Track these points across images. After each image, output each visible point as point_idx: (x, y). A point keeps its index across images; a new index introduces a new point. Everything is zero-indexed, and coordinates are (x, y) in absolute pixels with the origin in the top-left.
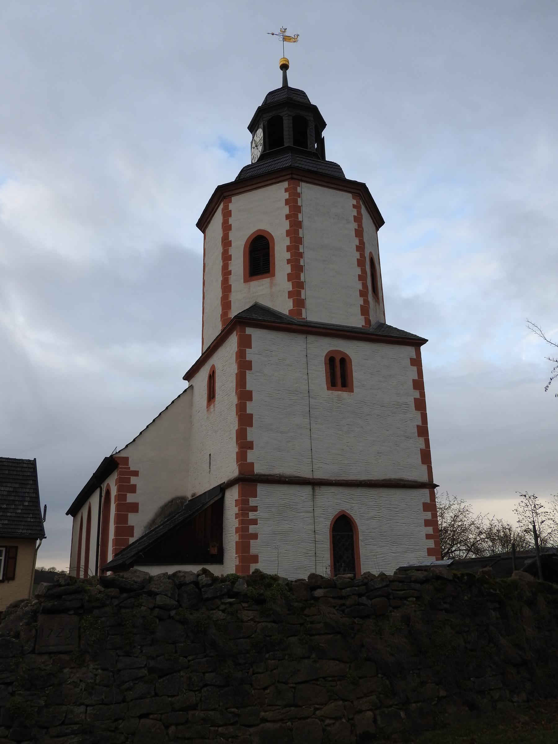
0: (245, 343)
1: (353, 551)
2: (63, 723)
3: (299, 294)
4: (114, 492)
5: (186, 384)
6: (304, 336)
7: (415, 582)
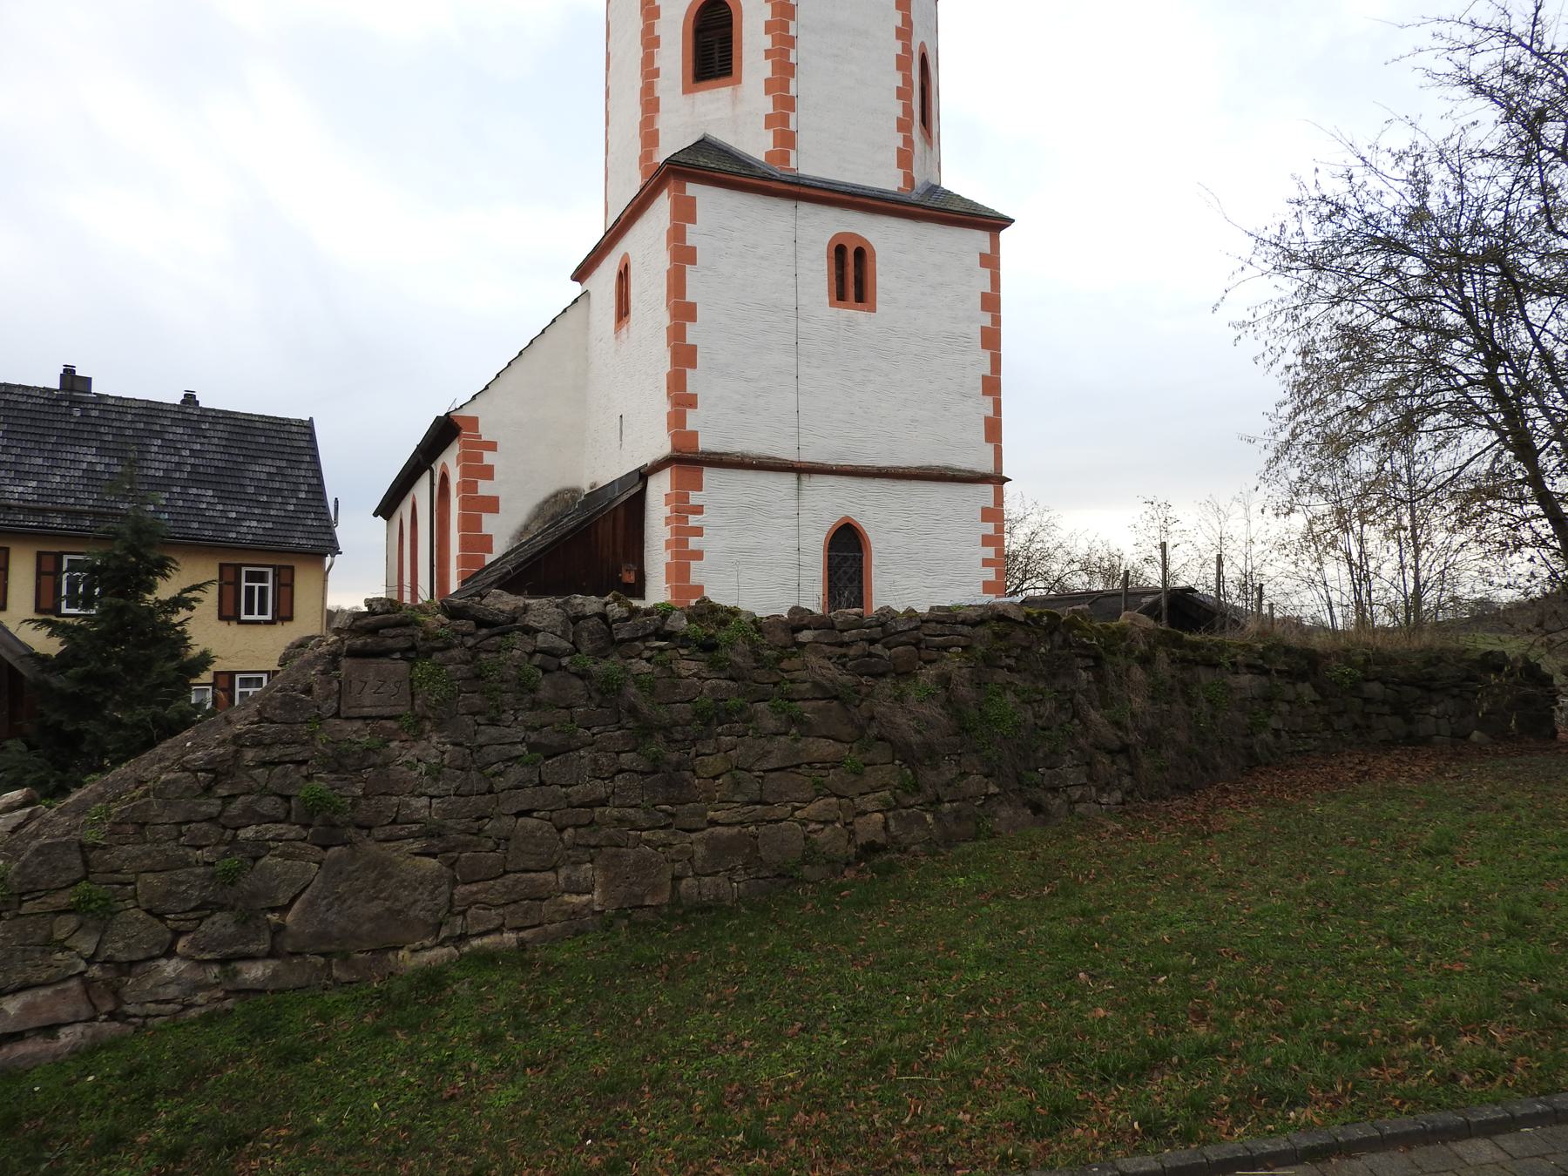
0: (684, 212)
1: (861, 582)
2: (394, 822)
3: (785, 120)
4: (455, 478)
5: (576, 289)
6: (793, 204)
7: (963, 623)
